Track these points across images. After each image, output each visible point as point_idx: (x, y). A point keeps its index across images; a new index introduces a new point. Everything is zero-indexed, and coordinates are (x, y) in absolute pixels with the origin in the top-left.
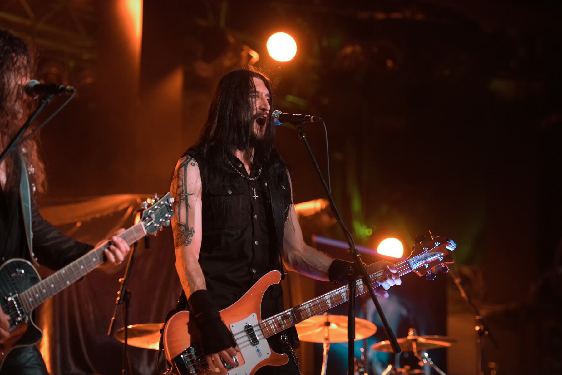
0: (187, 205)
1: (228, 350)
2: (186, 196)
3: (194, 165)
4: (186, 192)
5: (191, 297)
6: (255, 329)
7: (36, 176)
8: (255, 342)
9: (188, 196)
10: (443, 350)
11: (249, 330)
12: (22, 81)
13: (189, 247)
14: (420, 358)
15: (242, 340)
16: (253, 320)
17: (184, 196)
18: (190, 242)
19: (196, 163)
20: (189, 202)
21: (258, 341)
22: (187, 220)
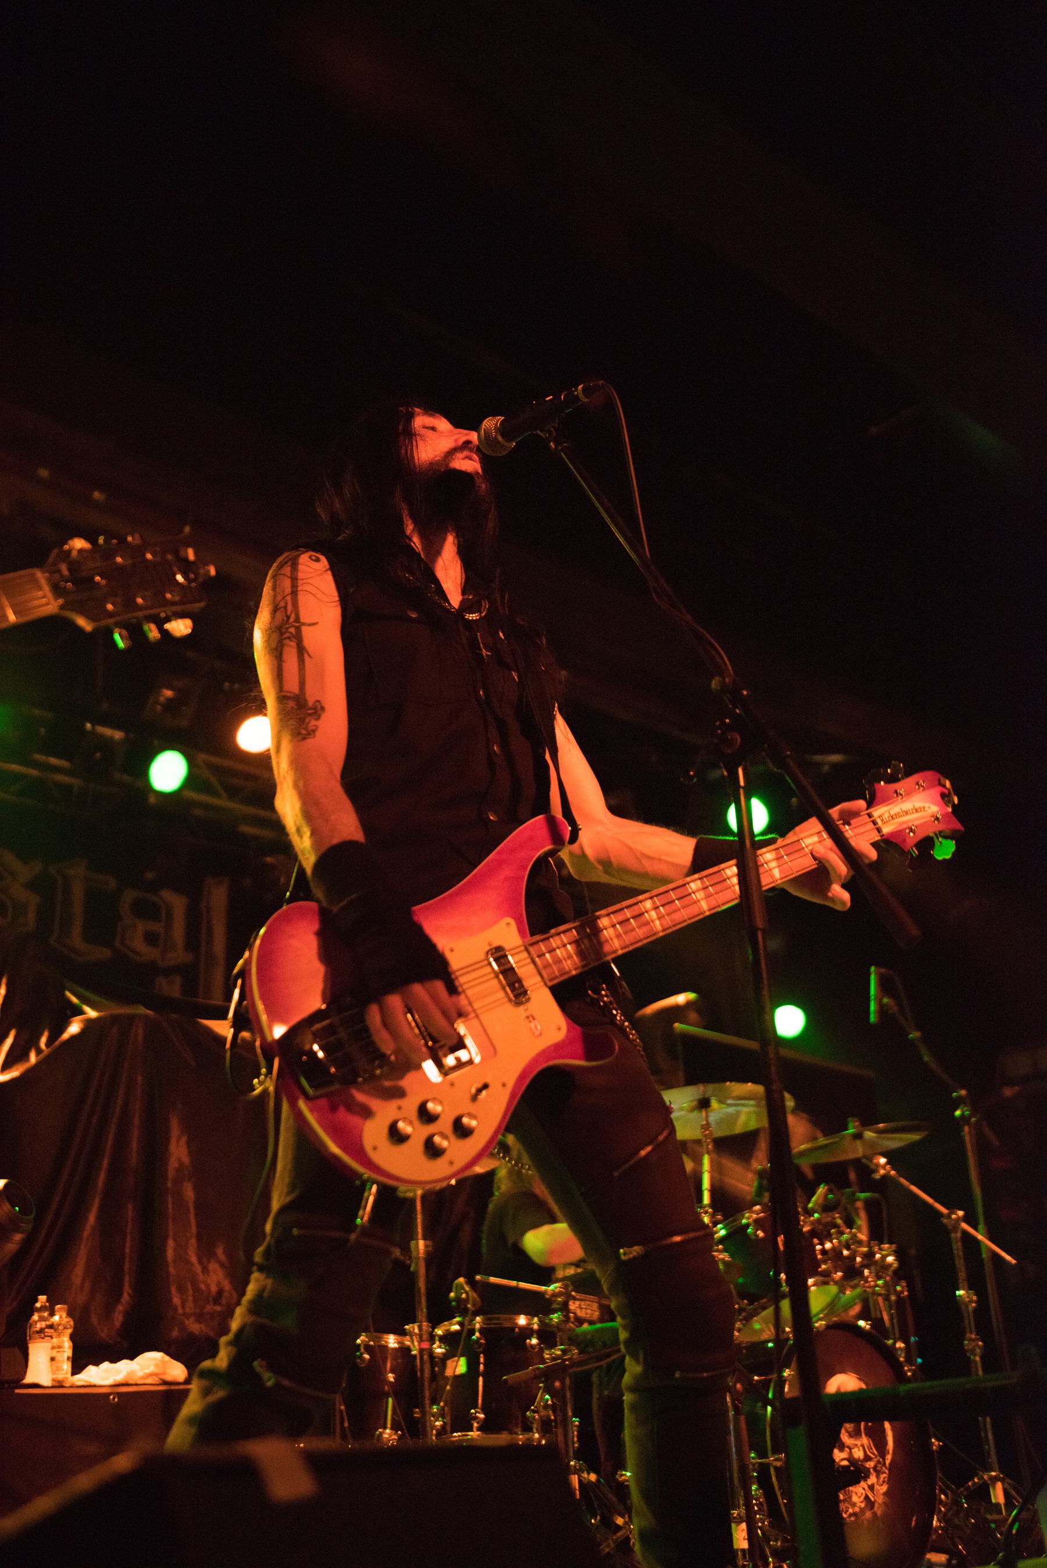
0: (301, 650)
2: (298, 629)
5: (317, 866)
7: (645, 862)
8: (518, 993)
9: (304, 629)
10: (615, 1533)
12: (770, 861)
13: (613, 860)
15: (480, 987)
16: (507, 933)
17: (292, 630)
18: (314, 731)
20: (306, 643)
22: (302, 684)
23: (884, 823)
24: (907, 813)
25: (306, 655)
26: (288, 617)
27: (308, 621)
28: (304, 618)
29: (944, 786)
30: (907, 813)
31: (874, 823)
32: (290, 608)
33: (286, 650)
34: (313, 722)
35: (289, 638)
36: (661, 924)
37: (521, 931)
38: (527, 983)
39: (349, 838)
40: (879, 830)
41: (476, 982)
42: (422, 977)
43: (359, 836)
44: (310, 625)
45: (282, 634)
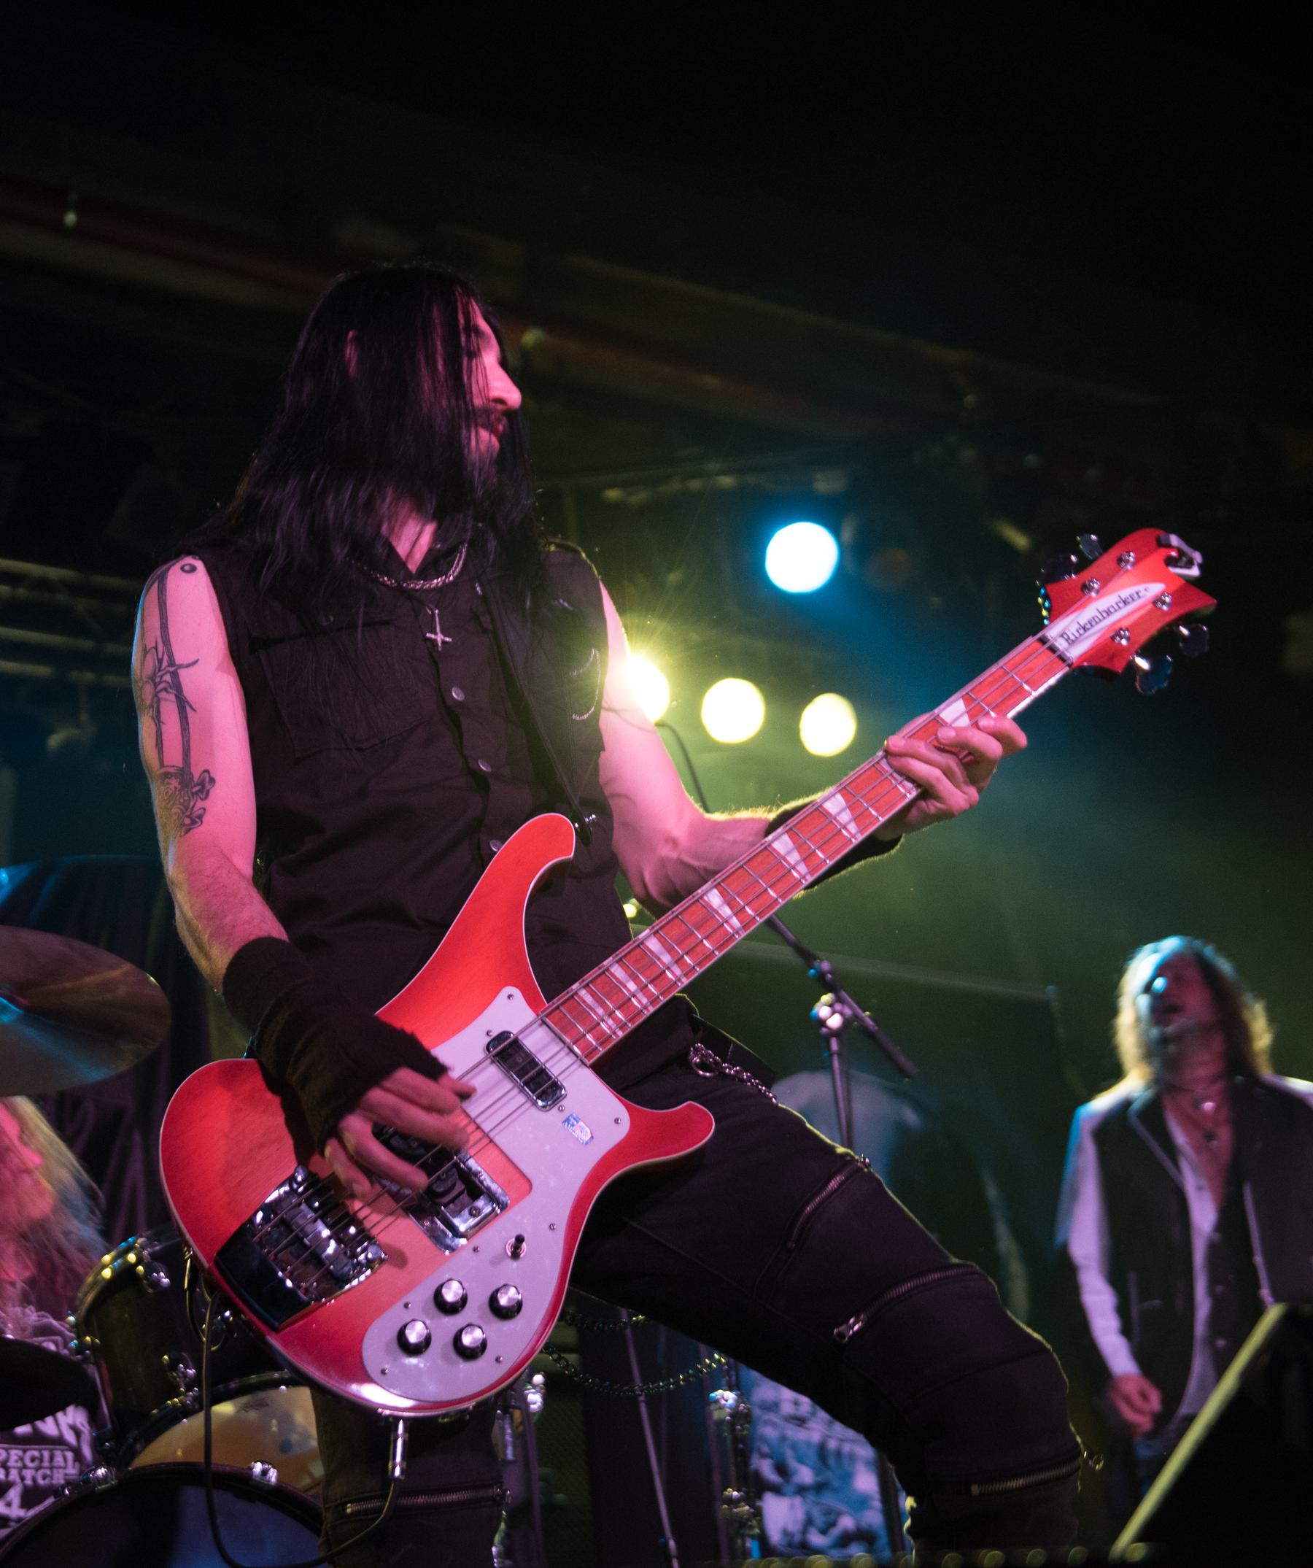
0: (182, 703)
1: (387, 1084)
2: (175, 675)
3: (193, 569)
4: (172, 662)
6: (542, 1058)
8: (542, 1087)
9: (182, 673)
11: (507, 1052)
14: (838, 1007)
15: (497, 1106)
16: (510, 1011)
17: (167, 678)
18: (200, 817)
19: (199, 564)
20: (188, 692)
21: (556, 1086)
23: (1072, 642)
24: (1109, 613)
25: (188, 709)
26: (160, 661)
27: (186, 662)
28: (180, 658)
29: (1169, 546)
30: (1109, 613)
31: (1053, 649)
32: (160, 648)
33: (163, 705)
34: (200, 804)
35: (165, 689)
36: (741, 922)
37: (532, 1002)
38: (554, 1070)
39: (263, 934)
40: (1062, 659)
41: (498, 1105)
42: (377, 1076)
43: (276, 930)
44: (188, 666)
45: (156, 685)
